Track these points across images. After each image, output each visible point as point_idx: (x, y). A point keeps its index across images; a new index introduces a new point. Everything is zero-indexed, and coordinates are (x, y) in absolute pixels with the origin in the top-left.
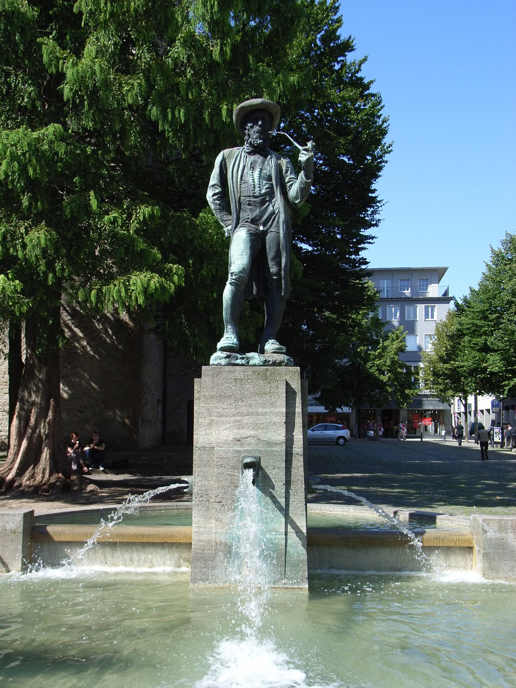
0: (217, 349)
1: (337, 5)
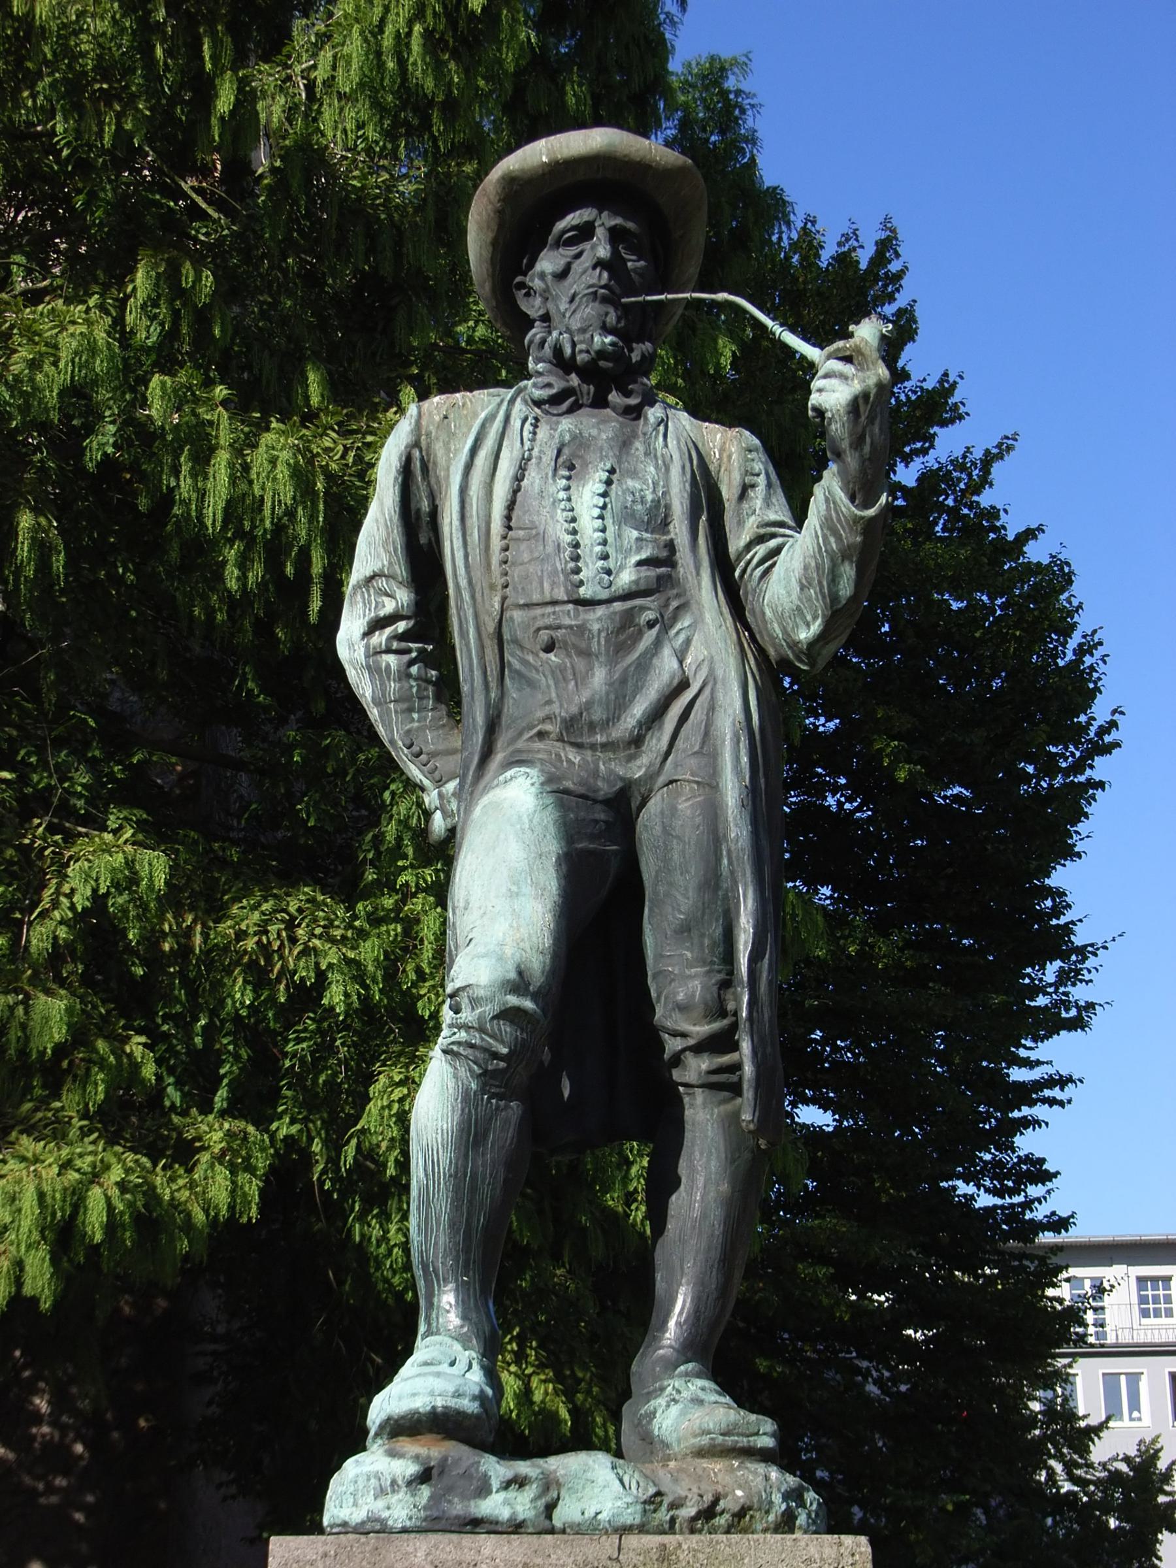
0: (366, 1432)
1: (894, 267)
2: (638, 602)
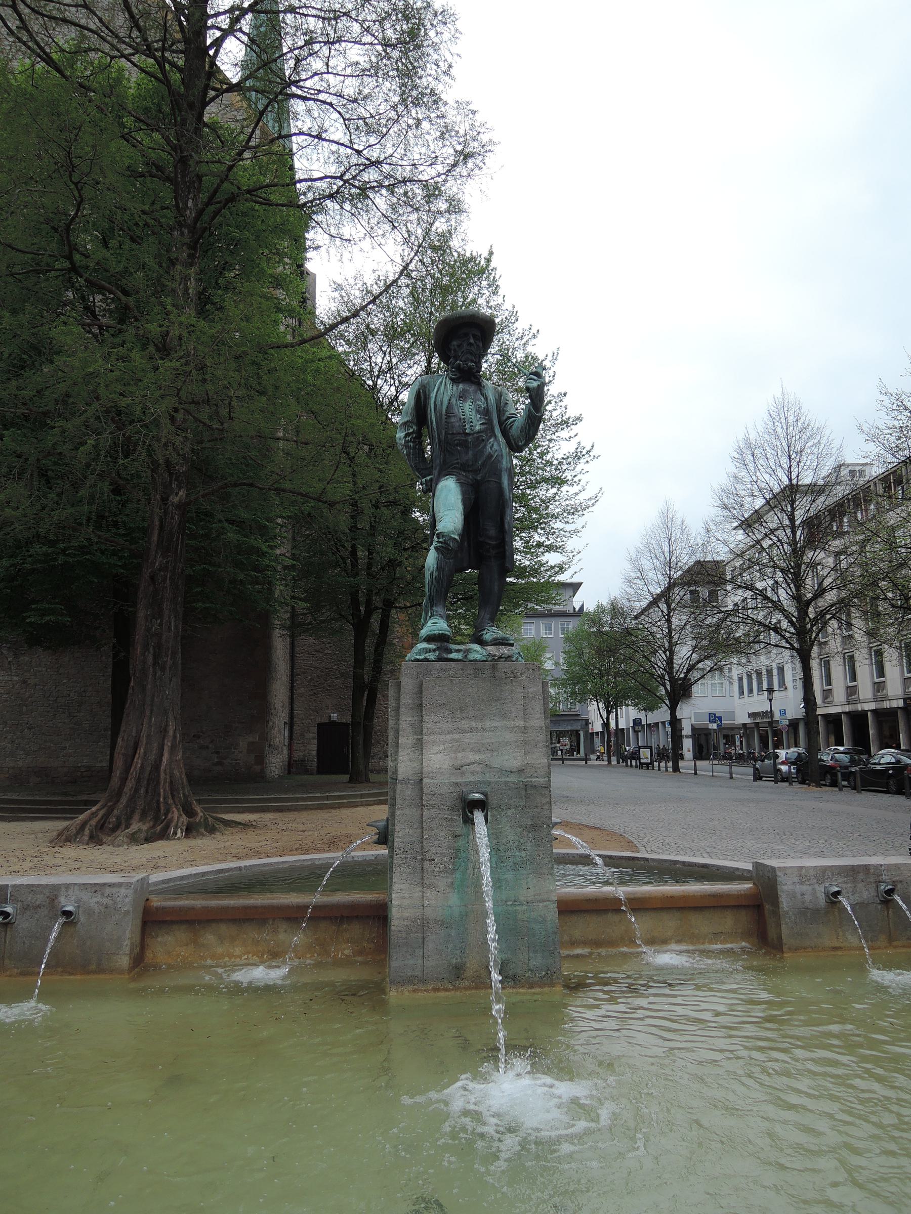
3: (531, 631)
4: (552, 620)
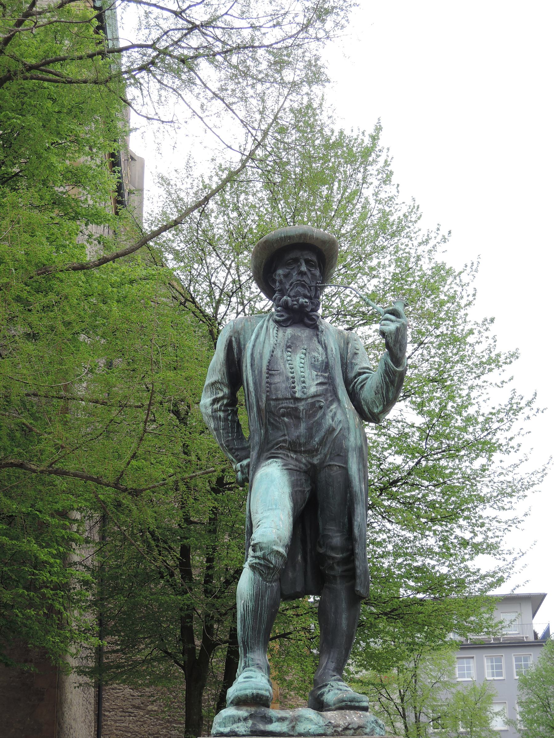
2: (318, 399)
3: (469, 671)
4: (502, 653)
